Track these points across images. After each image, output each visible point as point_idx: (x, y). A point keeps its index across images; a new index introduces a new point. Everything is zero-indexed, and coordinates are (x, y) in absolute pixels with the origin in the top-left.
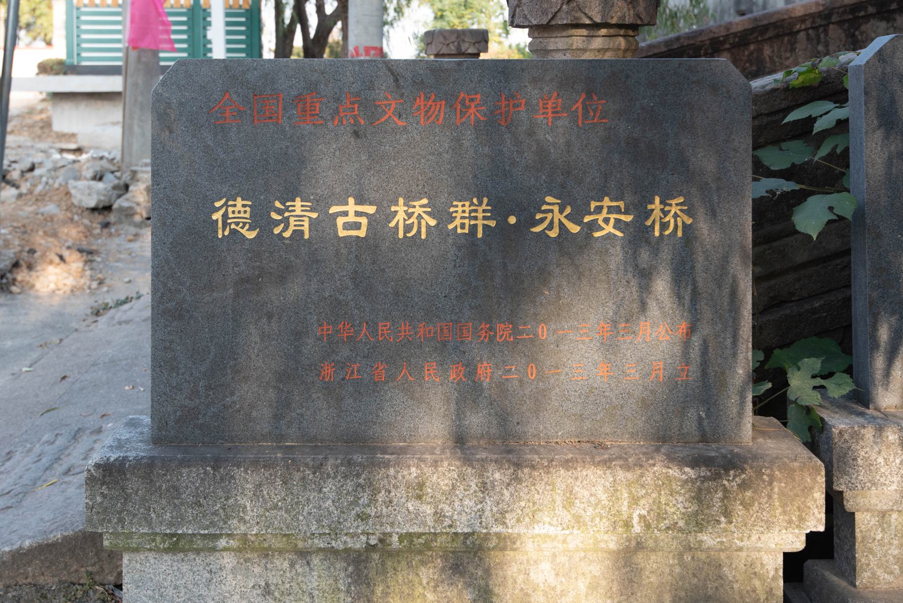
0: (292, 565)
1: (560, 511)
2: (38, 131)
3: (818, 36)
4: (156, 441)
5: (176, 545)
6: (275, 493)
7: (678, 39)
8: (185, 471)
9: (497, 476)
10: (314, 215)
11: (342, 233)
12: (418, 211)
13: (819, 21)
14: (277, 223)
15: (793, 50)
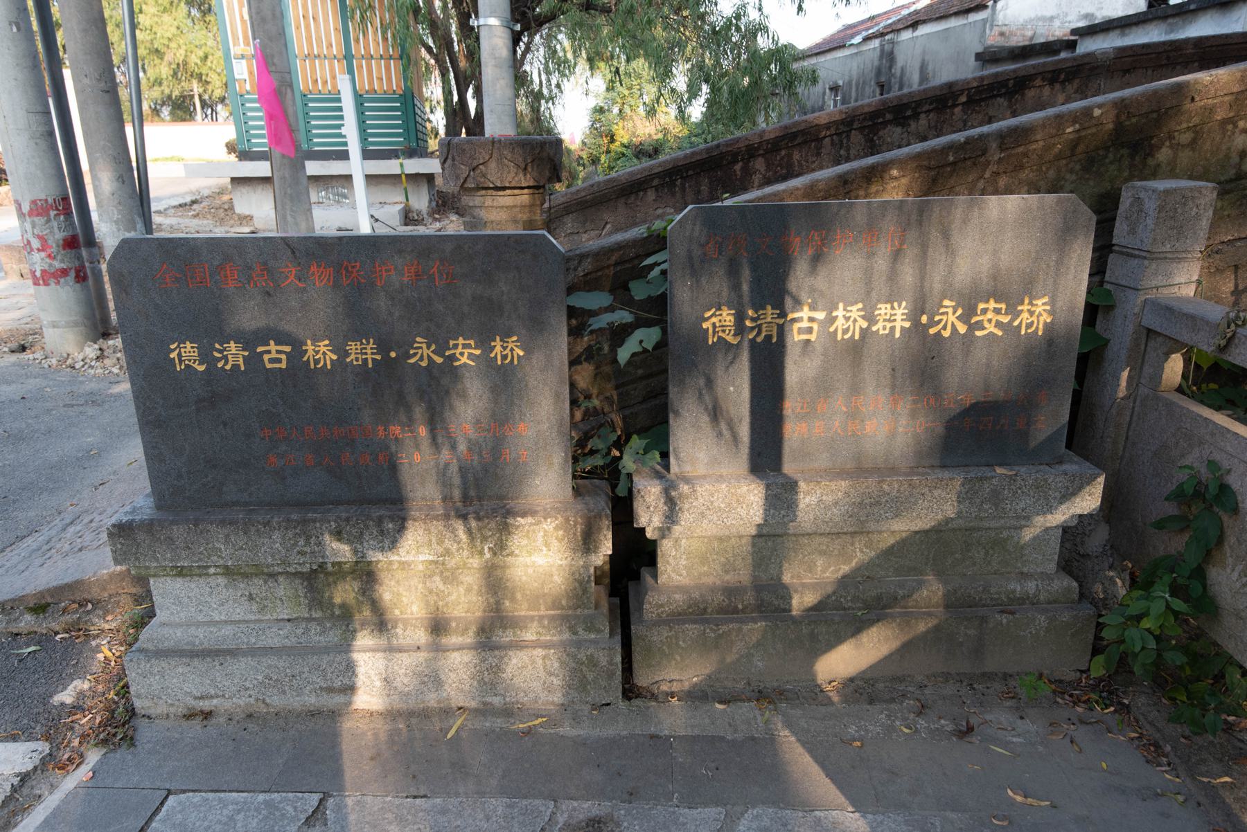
0: (266, 582)
1: (435, 546)
2: (221, 213)
3: (841, 141)
4: (159, 507)
5: (181, 572)
6: (241, 539)
7: (718, 146)
8: (175, 528)
9: (390, 526)
10: (246, 353)
11: (269, 366)
12: (323, 349)
13: (842, 128)
14: (219, 360)
15: (818, 154)
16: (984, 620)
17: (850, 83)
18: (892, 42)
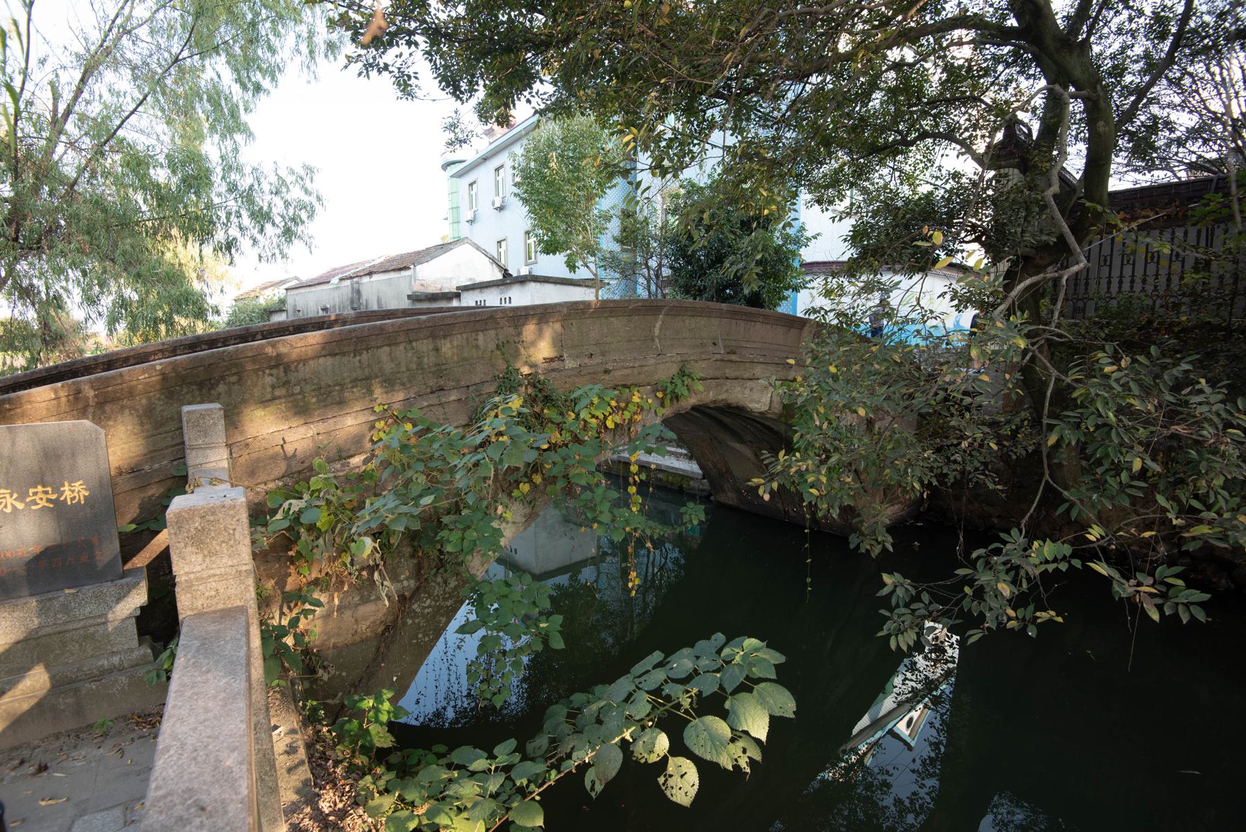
16: (77, 690)
17: (334, 307)
18: (358, 283)
